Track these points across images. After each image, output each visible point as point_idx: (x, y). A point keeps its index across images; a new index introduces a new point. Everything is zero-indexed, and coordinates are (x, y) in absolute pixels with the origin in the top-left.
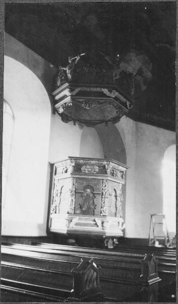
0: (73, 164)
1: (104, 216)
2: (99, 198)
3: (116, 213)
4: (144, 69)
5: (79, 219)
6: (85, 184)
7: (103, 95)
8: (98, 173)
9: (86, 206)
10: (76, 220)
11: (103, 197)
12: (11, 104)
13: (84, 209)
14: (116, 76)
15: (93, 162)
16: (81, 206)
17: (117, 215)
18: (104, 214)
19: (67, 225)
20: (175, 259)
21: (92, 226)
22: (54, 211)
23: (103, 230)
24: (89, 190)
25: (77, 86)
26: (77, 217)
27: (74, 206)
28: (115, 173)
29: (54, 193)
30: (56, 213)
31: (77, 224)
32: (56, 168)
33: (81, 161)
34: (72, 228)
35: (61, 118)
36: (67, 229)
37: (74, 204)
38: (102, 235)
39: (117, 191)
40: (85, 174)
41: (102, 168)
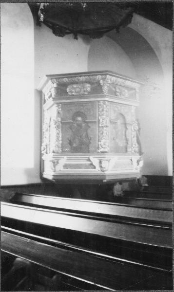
0: (55, 85)
1: (103, 152)
2: (92, 126)
3: (126, 148)
5: (69, 159)
6: (74, 109)
8: (89, 93)
9: (77, 141)
10: (64, 160)
11: (100, 125)
13: (74, 145)
15: (82, 78)
16: (70, 141)
17: (129, 150)
18: (102, 150)
19: (52, 169)
20: (2, 227)
21: (86, 167)
22: (45, 150)
23: (102, 173)
24: (79, 119)
26: (65, 157)
27: (61, 142)
28: (118, 90)
29: (45, 126)
30: (47, 153)
31: (66, 166)
33: (65, 80)
35: (51, 31)
37: (60, 139)
38: (102, 178)
39: (126, 116)
40: (73, 97)
41: (96, 85)
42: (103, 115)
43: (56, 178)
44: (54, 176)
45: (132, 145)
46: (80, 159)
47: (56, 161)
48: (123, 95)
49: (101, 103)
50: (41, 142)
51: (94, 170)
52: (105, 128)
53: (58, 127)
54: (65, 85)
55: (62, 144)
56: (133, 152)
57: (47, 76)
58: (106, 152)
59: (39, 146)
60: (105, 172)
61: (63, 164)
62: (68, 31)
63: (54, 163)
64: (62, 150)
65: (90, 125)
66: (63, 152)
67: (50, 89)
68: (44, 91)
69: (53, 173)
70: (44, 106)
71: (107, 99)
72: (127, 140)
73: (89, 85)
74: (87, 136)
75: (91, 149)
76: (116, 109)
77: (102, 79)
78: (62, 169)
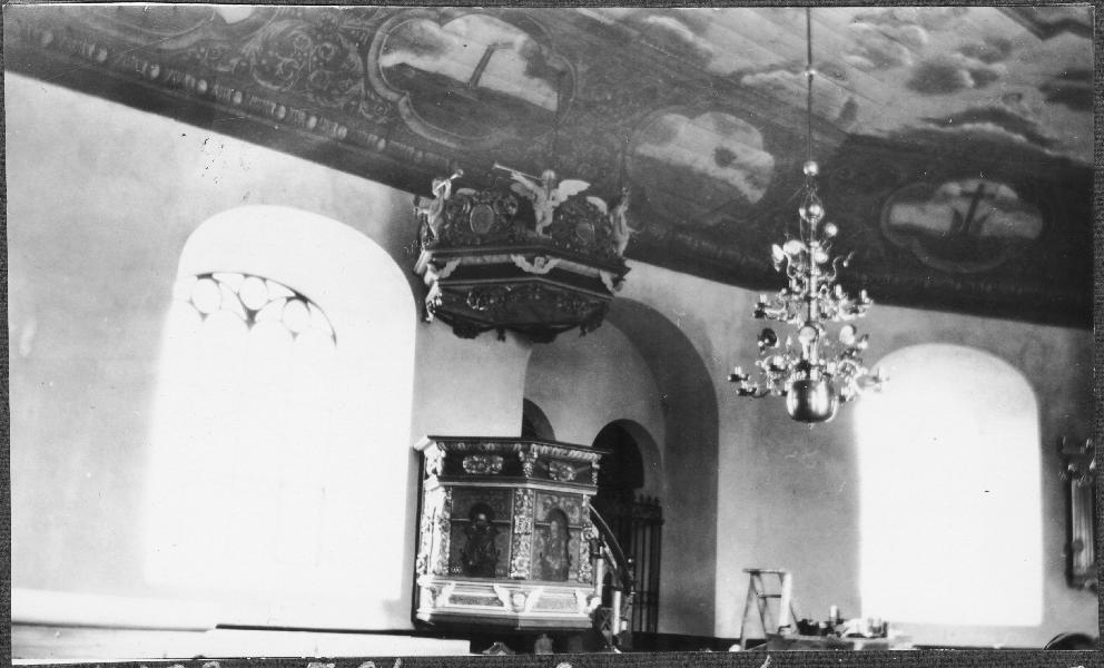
0: (443, 454)
1: (517, 578)
4: (735, 147)
6: (473, 501)
7: (513, 270)
10: (450, 588)
11: (516, 531)
12: (324, 308)
14: (544, 218)
16: (464, 555)
22: (423, 568)
25: (451, 256)
26: (454, 583)
27: (448, 556)
29: (425, 522)
30: (425, 572)
31: (454, 599)
33: (461, 446)
34: (442, 610)
37: (447, 550)
38: (512, 623)
40: (471, 478)
42: (521, 513)
43: (438, 618)
44: (432, 615)
45: (579, 566)
46: (478, 589)
47: (437, 590)
48: (564, 477)
49: (520, 493)
50: (417, 551)
51: (500, 608)
52: (523, 537)
53: (444, 529)
54: (462, 455)
55: (450, 560)
56: (580, 579)
57: (430, 437)
58: (522, 579)
59: (413, 558)
60: (519, 614)
61: (449, 595)
62: (485, 326)
63: (433, 592)
64: (449, 570)
65: (499, 529)
66: (451, 575)
67: (435, 457)
68: (426, 453)
69: (432, 611)
70: (425, 482)
71: (529, 485)
72: (569, 558)
73: (502, 459)
74: (493, 549)
75: (499, 571)
76: (549, 502)
77: (523, 450)
78: (447, 604)
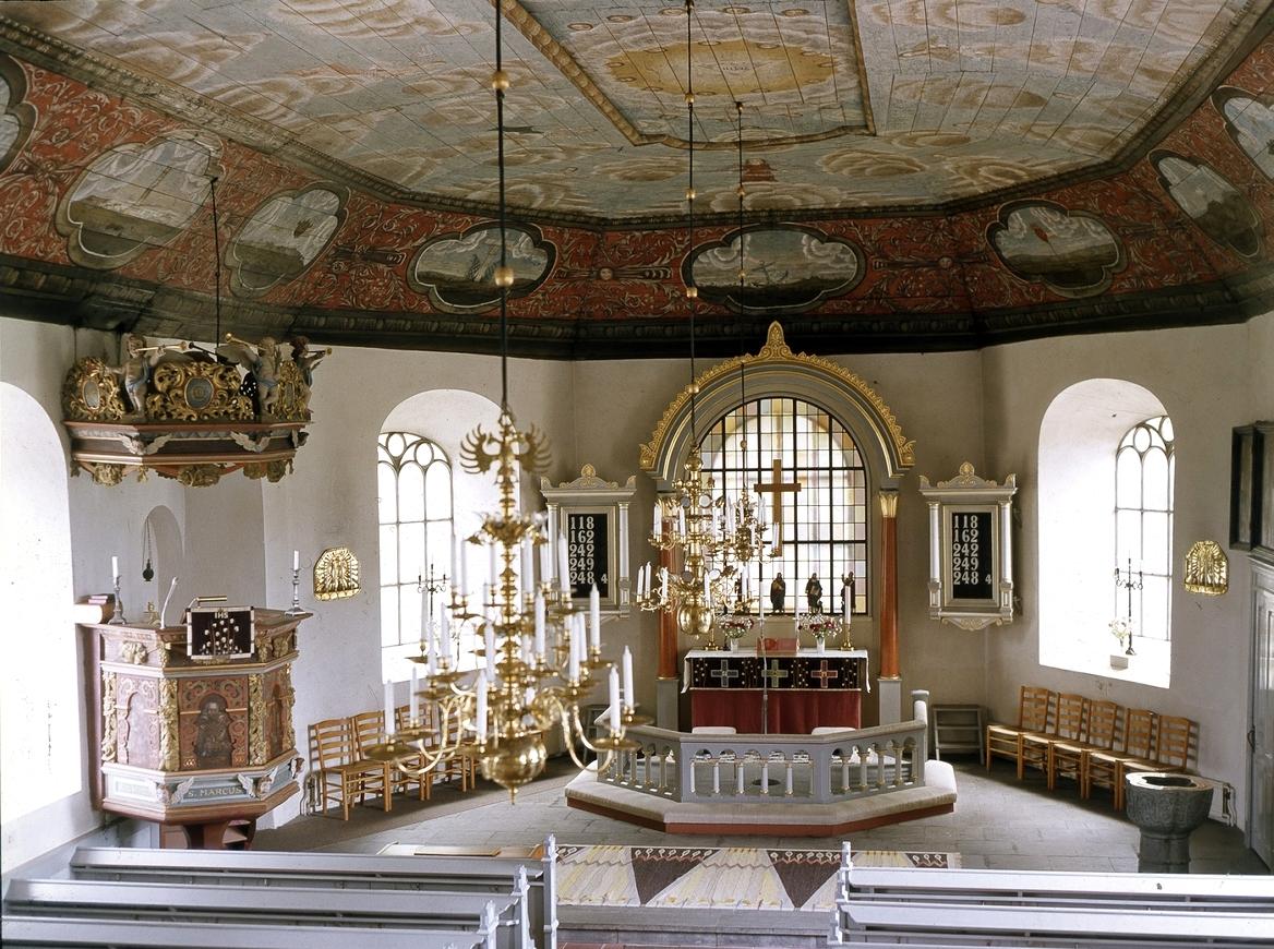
10: (187, 783)
22: (113, 755)
24: (214, 706)
29: (784, 938)
32: (102, 638)
36: (1206, 203)
